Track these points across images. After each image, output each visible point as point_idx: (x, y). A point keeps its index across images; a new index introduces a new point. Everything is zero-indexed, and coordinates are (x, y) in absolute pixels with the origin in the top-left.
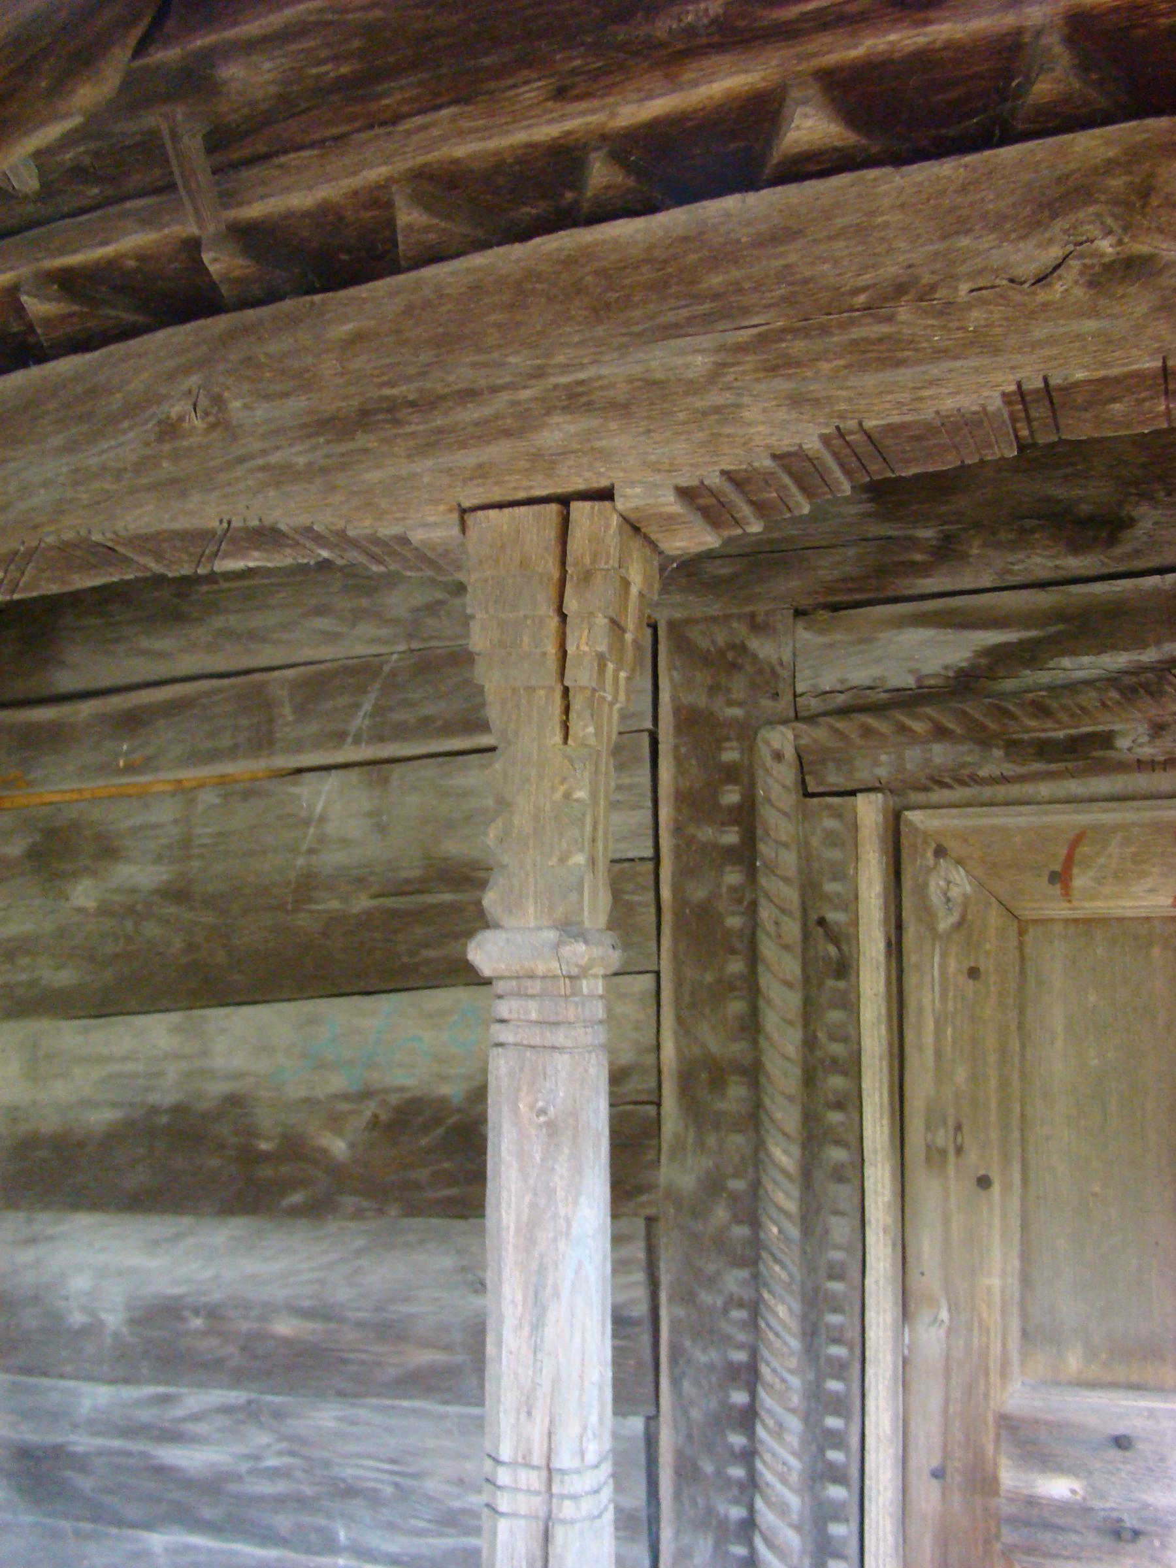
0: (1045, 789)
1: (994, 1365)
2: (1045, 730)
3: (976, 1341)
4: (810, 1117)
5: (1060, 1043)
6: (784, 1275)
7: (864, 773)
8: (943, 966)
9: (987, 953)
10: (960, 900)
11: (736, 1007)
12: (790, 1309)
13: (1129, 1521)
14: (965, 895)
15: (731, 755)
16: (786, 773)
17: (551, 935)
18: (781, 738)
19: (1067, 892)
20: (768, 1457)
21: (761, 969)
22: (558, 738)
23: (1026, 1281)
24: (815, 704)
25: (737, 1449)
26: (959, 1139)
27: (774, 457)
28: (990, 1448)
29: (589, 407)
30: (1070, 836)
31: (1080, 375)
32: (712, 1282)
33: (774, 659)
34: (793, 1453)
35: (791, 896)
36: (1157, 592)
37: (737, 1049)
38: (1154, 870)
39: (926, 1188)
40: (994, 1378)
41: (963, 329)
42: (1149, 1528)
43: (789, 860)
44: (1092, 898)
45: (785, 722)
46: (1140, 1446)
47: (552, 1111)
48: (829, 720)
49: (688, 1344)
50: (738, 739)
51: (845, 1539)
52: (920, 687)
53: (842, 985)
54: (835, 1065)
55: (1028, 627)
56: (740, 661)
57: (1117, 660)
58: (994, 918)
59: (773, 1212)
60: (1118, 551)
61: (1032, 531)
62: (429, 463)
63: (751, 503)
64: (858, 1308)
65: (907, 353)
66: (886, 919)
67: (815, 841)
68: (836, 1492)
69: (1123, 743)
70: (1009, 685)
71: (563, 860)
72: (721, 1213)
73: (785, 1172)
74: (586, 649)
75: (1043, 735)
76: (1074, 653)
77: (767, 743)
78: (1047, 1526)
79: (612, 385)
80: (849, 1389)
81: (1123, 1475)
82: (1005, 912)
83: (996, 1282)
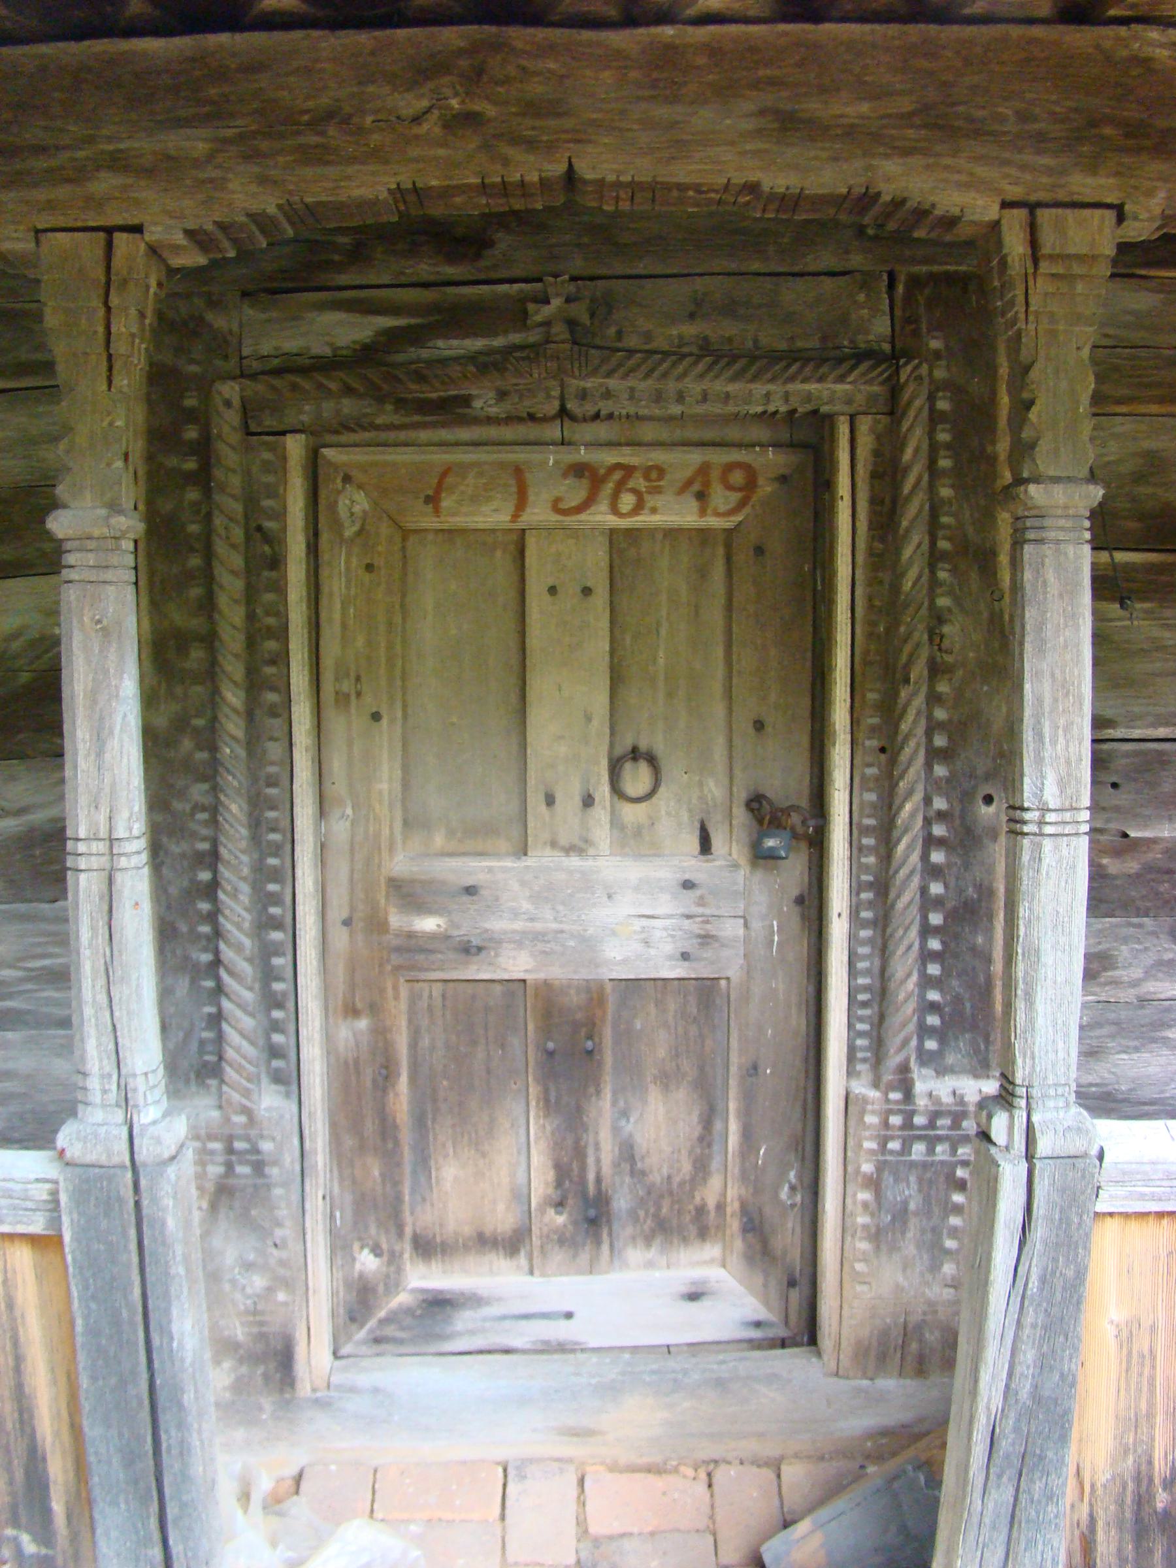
0: (424, 435)
1: (384, 845)
2: (423, 392)
4: (251, 672)
6: (235, 783)
7: (290, 420)
8: (348, 562)
9: (379, 553)
10: (361, 514)
11: (196, 592)
12: (240, 807)
14: (364, 512)
15: (190, 402)
16: (232, 417)
17: (103, 512)
18: (230, 390)
19: (437, 511)
20: (227, 912)
21: (215, 564)
22: (105, 387)
23: (406, 785)
24: (256, 365)
25: (204, 912)
27: (248, 215)
28: (383, 901)
29: (126, 169)
31: (434, 183)
32: (182, 794)
34: (246, 909)
35: (237, 508)
36: (507, 296)
37: (196, 623)
39: (336, 724)
40: (385, 854)
41: (367, 145)
43: (235, 481)
44: (453, 515)
45: (234, 378)
46: (483, 892)
47: (105, 622)
48: (266, 377)
49: (165, 839)
51: (283, 967)
53: (274, 574)
54: (270, 633)
55: (413, 316)
57: (476, 344)
58: (385, 529)
59: (227, 739)
62: (12, 195)
63: (230, 239)
64: (288, 806)
65: (332, 157)
66: (306, 528)
67: (255, 469)
68: (276, 936)
69: (477, 404)
70: (400, 358)
71: (109, 465)
72: (187, 744)
73: (235, 710)
74: (124, 330)
75: (422, 396)
76: (447, 337)
77: (220, 393)
78: (422, 950)
79: (141, 156)
80: (283, 863)
81: (471, 912)
83: (385, 786)
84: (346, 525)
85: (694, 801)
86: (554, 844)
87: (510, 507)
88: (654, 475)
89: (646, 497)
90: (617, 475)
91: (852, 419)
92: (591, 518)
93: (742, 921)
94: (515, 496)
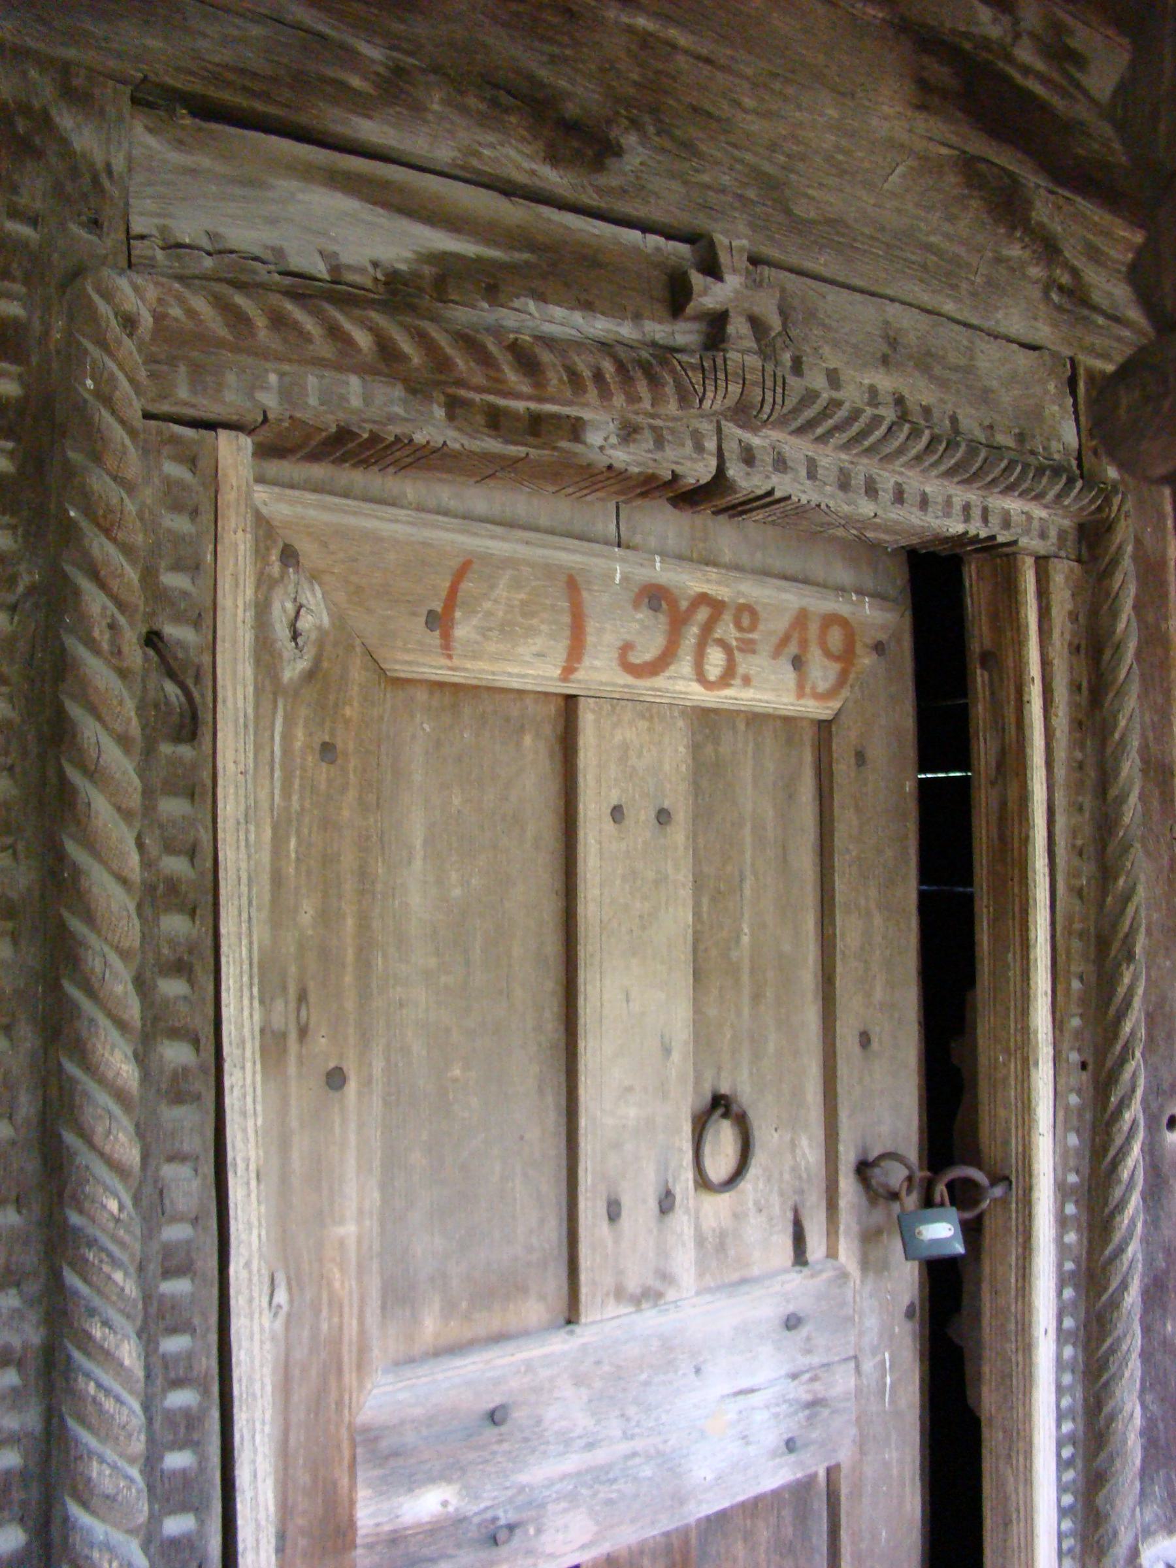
1: (348, 1359)
3: (325, 1326)
5: (418, 864)
8: (287, 737)
9: (347, 722)
13: (505, 1517)
26: (304, 1013)
30: (455, 563)
33: (99, 157)
38: (544, 627)
40: (350, 1377)
42: (524, 1515)
44: (475, 657)
50: (26, 282)
52: (333, 282)
53: (185, 751)
55: (488, 242)
56: (38, 141)
60: (602, 180)
61: (507, 110)
69: (594, 438)
73: (120, 1096)
82: (371, 664)
84: (286, 655)
85: (787, 1176)
86: (619, 1293)
87: (560, 649)
88: (746, 622)
89: (738, 656)
90: (703, 614)
91: (1042, 561)
92: (669, 685)
93: (852, 1364)
94: (568, 633)
